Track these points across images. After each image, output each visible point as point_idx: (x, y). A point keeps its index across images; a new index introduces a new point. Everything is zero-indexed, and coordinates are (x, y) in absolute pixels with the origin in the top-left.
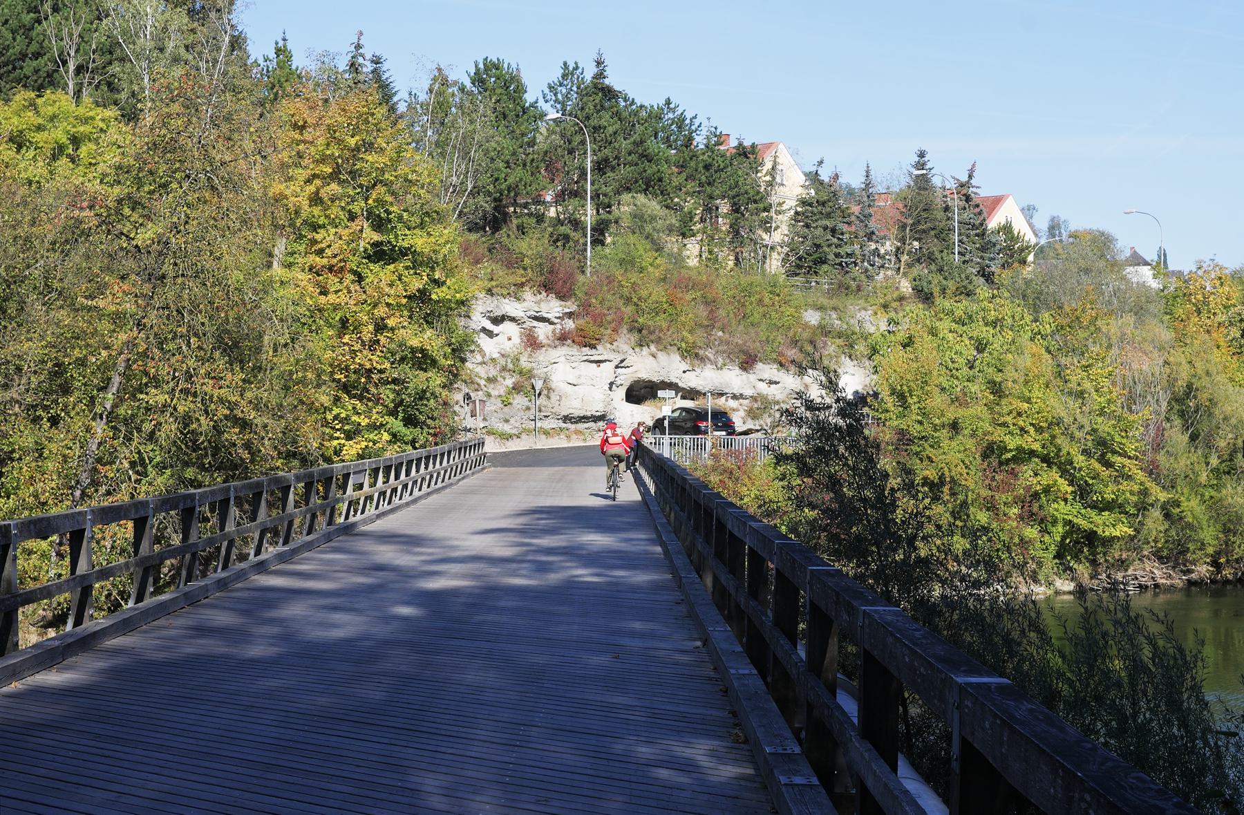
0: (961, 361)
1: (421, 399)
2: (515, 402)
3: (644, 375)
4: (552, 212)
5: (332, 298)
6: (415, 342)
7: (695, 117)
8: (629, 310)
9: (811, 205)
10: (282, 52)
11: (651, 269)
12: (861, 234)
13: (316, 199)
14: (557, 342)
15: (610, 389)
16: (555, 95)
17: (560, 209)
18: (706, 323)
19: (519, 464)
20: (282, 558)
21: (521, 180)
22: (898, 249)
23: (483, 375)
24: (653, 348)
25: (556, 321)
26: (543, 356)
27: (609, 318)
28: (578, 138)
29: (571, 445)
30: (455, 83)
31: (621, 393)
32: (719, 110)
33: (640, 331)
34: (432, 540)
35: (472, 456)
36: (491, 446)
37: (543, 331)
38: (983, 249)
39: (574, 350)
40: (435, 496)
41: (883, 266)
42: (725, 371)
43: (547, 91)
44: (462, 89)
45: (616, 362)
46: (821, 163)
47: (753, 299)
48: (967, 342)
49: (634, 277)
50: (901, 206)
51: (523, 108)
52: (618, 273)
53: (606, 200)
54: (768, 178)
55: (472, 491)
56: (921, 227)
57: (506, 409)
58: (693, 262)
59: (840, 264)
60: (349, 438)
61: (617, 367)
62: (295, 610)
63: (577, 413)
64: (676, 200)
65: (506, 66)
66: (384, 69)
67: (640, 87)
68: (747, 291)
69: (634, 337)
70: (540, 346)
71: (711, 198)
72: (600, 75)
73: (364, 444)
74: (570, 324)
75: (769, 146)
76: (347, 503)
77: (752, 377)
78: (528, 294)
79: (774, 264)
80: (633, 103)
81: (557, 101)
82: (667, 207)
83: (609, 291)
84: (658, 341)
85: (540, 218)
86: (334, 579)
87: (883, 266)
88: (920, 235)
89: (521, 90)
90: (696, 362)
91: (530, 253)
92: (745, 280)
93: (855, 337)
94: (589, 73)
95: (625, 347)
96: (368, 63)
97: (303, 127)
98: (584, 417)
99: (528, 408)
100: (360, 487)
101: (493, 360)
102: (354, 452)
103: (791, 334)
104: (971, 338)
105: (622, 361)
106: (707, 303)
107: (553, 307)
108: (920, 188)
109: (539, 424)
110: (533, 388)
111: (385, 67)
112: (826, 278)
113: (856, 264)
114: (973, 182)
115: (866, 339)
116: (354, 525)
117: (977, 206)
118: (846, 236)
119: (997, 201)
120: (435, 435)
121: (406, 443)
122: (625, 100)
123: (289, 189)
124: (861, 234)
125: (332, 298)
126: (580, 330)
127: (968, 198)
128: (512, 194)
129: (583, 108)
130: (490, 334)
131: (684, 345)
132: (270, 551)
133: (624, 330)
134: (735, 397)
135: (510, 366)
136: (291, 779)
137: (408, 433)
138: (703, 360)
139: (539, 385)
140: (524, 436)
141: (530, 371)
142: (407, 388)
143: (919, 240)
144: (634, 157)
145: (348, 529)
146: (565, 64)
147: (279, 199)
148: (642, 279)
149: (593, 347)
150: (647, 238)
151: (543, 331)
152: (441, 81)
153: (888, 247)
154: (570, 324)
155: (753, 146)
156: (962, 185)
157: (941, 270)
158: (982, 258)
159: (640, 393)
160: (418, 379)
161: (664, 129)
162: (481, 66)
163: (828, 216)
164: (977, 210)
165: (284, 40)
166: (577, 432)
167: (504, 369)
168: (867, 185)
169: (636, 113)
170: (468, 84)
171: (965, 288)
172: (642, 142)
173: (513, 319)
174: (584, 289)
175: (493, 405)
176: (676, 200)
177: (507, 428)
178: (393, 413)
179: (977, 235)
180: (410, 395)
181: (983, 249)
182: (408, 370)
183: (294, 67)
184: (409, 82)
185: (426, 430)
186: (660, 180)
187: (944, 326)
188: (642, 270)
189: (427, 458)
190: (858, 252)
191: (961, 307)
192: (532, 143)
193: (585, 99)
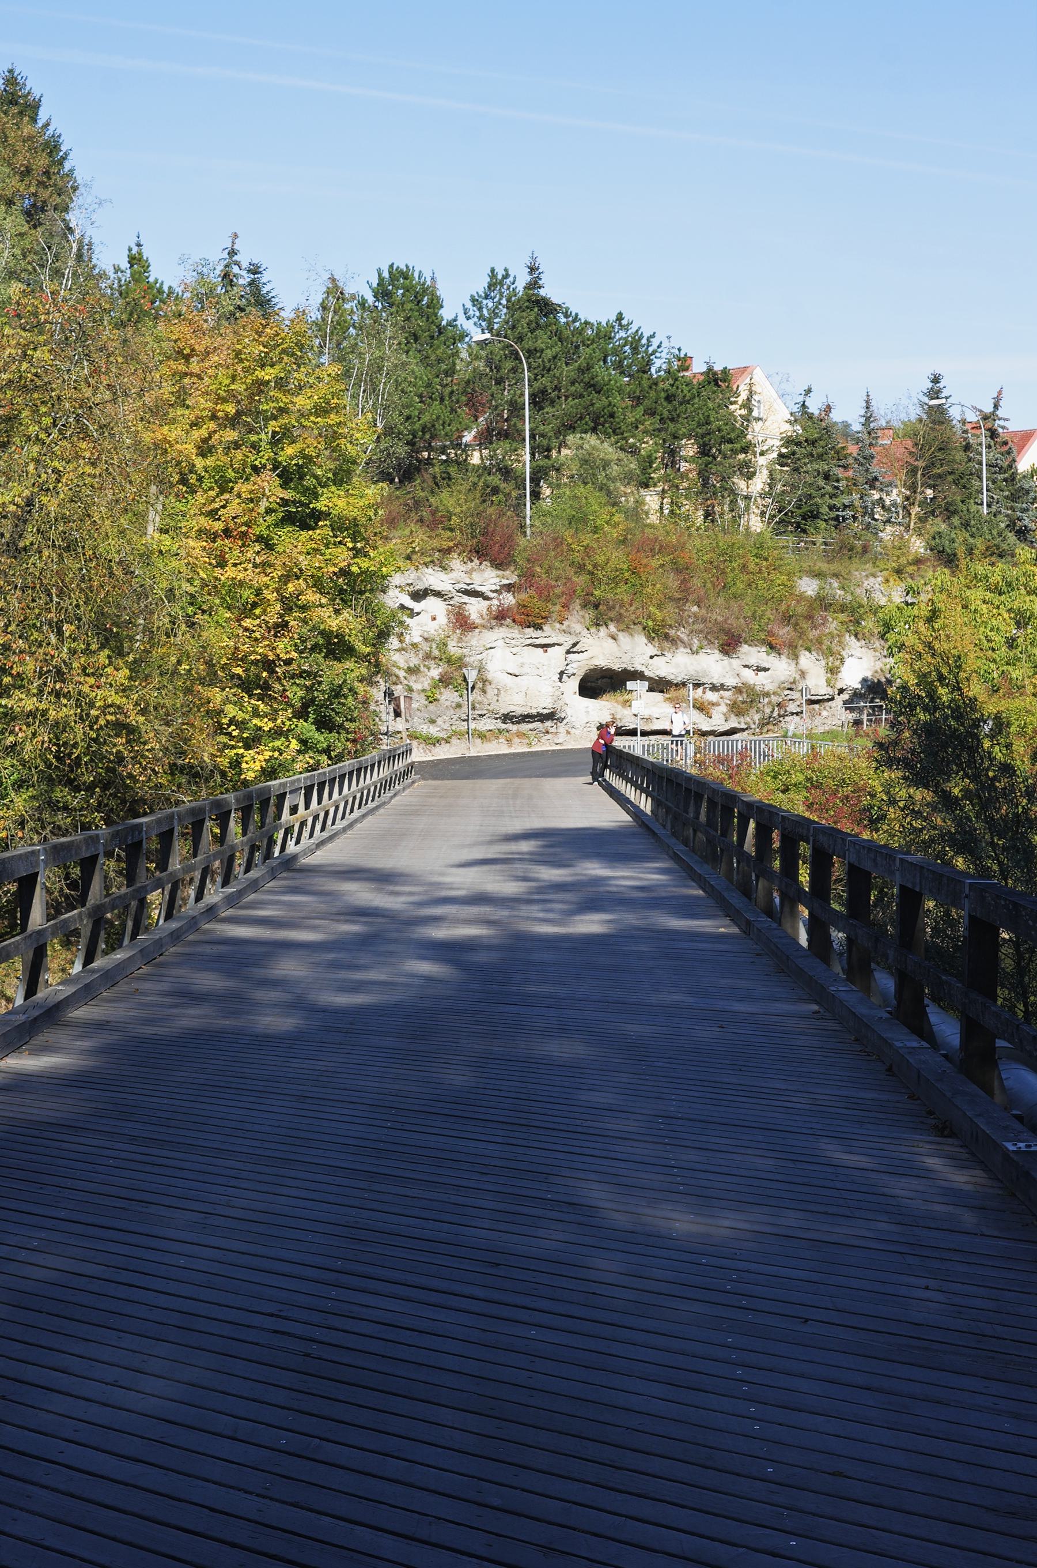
0: (999, 639)
1: (337, 695)
2: (443, 698)
3: (602, 662)
4: (475, 459)
5: (230, 572)
6: (334, 624)
7: (653, 336)
8: (581, 580)
9: (798, 444)
10: (135, 260)
11: (607, 528)
12: (861, 480)
13: (205, 449)
14: (494, 622)
15: (560, 679)
16: (480, 309)
17: (485, 452)
18: (677, 595)
19: (454, 776)
20: (231, 901)
21: (438, 418)
22: (907, 498)
23: (402, 664)
24: (612, 628)
25: (492, 595)
26: (477, 640)
27: (557, 591)
28: (508, 365)
29: (512, 751)
30: (353, 297)
31: (574, 684)
32: (684, 328)
33: (596, 606)
34: (407, 875)
35: (400, 765)
36: (419, 755)
37: (475, 608)
38: (1014, 498)
39: (515, 632)
40: (370, 818)
41: (889, 521)
42: (702, 656)
43: (469, 305)
44: (363, 304)
45: (567, 646)
46: (809, 391)
47: (734, 564)
48: (1006, 616)
49: (587, 539)
50: (909, 444)
51: (439, 326)
52: (568, 534)
53: (545, 442)
54: (744, 412)
55: (414, 812)
56: (936, 471)
57: (432, 707)
58: (654, 519)
59: (837, 518)
60: (247, 747)
61: (568, 652)
62: (289, 968)
63: (519, 711)
64: (631, 440)
65: (416, 275)
66: (264, 280)
67: (584, 297)
68: (727, 554)
69: (589, 615)
70: (473, 627)
71: (675, 437)
72: (534, 284)
73: (267, 754)
74: (509, 599)
75: (744, 369)
76: (282, 832)
77: (736, 663)
78: (455, 562)
79: (756, 524)
80: (576, 319)
81: (481, 317)
82: (622, 449)
83: (556, 557)
84: (619, 619)
85: (462, 465)
86: (313, 928)
87: (889, 521)
88: (934, 481)
89: (436, 303)
90: (666, 644)
91: (458, 510)
92: (723, 540)
93: (862, 611)
94: (522, 280)
95: (578, 627)
96: (244, 273)
97: (187, 358)
98: (528, 716)
99: (459, 706)
100: (294, 810)
101: (414, 645)
102: (257, 766)
103: (784, 607)
104: (1010, 611)
105: (575, 645)
106: (678, 571)
107: (488, 578)
108: (934, 422)
109: (473, 725)
110: (465, 680)
111: (265, 277)
112: (820, 535)
113: (855, 518)
114: (1000, 413)
115: (875, 613)
116: (294, 857)
117: (1006, 443)
118: (842, 484)
119: (1026, 438)
120: (354, 741)
121: (320, 752)
122: (566, 316)
123: (173, 433)
124: (861, 480)
125: (230, 572)
126: (521, 606)
127: (993, 434)
128: (427, 436)
129: (514, 327)
130: (412, 614)
131: (650, 623)
132: (214, 894)
133: (576, 605)
134: (714, 688)
135: (436, 653)
136: (409, 1192)
137: (321, 739)
138: (674, 642)
139: (472, 676)
140: (454, 741)
141: (460, 659)
142: (320, 683)
143: (933, 487)
144: (578, 388)
145: (289, 863)
146: (493, 270)
147: (161, 447)
148: (597, 540)
149: (538, 627)
150: (601, 489)
151: (475, 608)
152: (335, 292)
153: (895, 496)
154: (509, 599)
155: (725, 371)
156: (986, 418)
157: (966, 525)
158: (1013, 509)
159: (598, 683)
160: (333, 672)
161: (615, 352)
162: (386, 274)
163: (821, 457)
164: (1006, 448)
165: (139, 245)
166: (521, 735)
167: (428, 656)
168: (868, 419)
169: (580, 332)
170: (370, 299)
171: (998, 547)
172: (589, 368)
173: (438, 594)
174: (526, 555)
175: (419, 701)
176: (631, 440)
177: (433, 731)
178: (301, 714)
179: (1005, 480)
180: (323, 692)
181: (1014, 498)
182: (321, 660)
183: (151, 280)
184: (295, 294)
185: (343, 735)
186: (612, 415)
187: (976, 596)
188: (595, 530)
189: (359, 770)
190: (857, 503)
191: (999, 571)
192: (451, 372)
193: (517, 314)
